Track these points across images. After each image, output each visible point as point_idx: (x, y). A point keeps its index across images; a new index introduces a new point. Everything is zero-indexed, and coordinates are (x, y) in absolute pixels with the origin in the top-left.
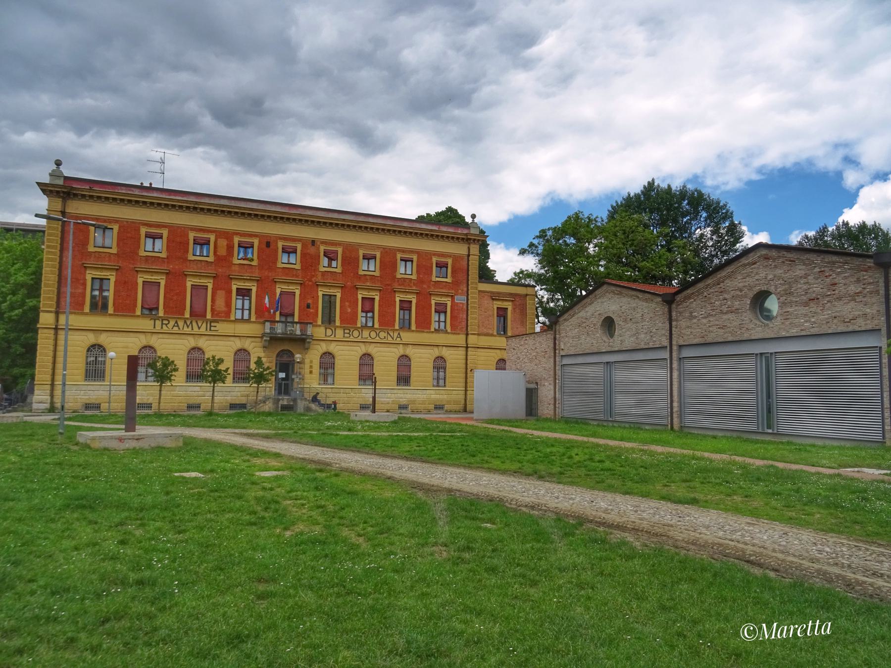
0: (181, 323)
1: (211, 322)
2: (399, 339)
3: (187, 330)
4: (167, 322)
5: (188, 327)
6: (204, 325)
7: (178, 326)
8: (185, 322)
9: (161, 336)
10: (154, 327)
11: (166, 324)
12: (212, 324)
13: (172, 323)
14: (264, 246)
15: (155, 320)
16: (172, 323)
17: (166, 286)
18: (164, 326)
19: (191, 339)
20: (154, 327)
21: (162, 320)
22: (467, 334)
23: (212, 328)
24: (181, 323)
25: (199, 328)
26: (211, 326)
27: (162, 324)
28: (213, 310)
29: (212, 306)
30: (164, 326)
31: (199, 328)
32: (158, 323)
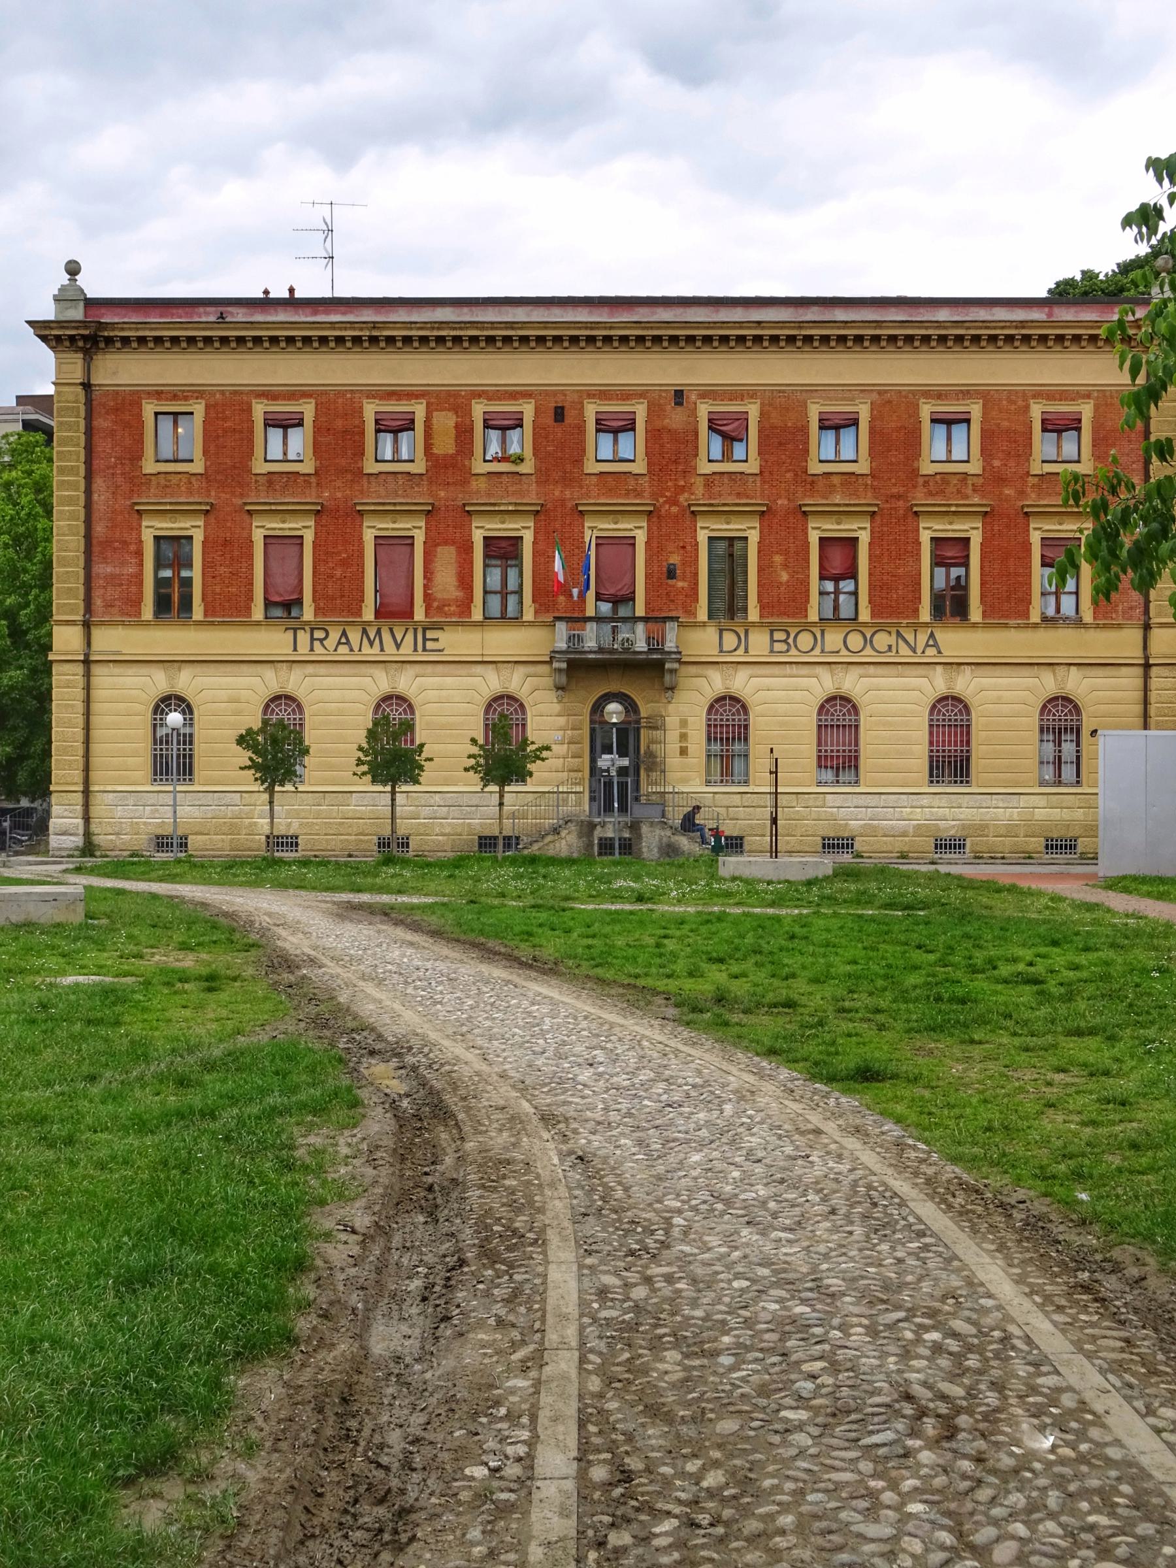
0: (354, 636)
1: (424, 630)
2: (343, 649)
3: (370, 652)
4: (782, 636)
5: (371, 644)
6: (410, 637)
7: (348, 643)
8: (365, 632)
9: (310, 669)
10: (295, 649)
11: (321, 640)
12: (429, 635)
13: (335, 635)
14: (549, 419)
15: (295, 630)
16: (335, 635)
17: (315, 545)
18: (317, 644)
19: (379, 674)
20: (295, 649)
21: (312, 630)
22: (1147, 627)
23: (429, 645)
24: (354, 636)
25: (398, 646)
26: (425, 639)
27: (312, 639)
28: (428, 598)
29: (426, 587)
30: (317, 644)
31: (398, 646)
32: (303, 637)
